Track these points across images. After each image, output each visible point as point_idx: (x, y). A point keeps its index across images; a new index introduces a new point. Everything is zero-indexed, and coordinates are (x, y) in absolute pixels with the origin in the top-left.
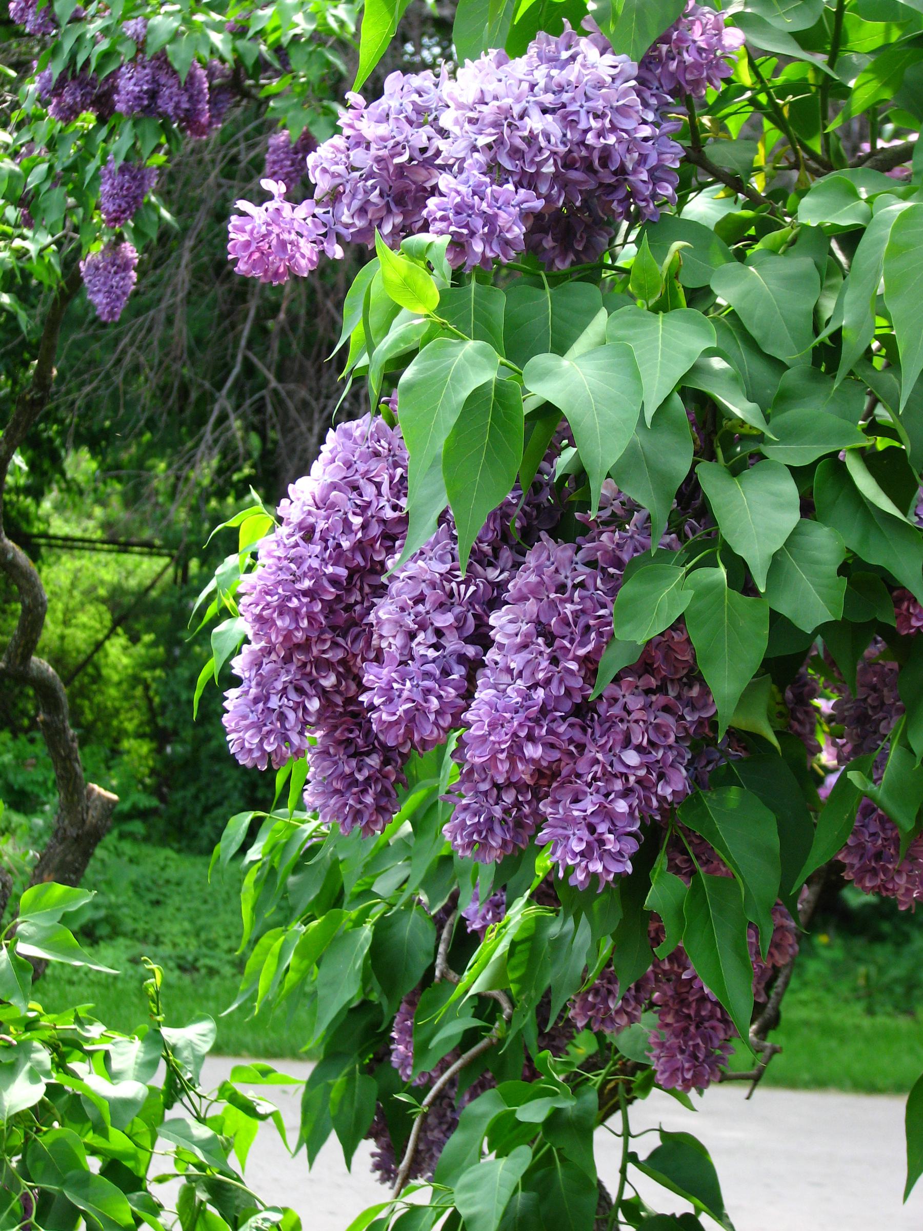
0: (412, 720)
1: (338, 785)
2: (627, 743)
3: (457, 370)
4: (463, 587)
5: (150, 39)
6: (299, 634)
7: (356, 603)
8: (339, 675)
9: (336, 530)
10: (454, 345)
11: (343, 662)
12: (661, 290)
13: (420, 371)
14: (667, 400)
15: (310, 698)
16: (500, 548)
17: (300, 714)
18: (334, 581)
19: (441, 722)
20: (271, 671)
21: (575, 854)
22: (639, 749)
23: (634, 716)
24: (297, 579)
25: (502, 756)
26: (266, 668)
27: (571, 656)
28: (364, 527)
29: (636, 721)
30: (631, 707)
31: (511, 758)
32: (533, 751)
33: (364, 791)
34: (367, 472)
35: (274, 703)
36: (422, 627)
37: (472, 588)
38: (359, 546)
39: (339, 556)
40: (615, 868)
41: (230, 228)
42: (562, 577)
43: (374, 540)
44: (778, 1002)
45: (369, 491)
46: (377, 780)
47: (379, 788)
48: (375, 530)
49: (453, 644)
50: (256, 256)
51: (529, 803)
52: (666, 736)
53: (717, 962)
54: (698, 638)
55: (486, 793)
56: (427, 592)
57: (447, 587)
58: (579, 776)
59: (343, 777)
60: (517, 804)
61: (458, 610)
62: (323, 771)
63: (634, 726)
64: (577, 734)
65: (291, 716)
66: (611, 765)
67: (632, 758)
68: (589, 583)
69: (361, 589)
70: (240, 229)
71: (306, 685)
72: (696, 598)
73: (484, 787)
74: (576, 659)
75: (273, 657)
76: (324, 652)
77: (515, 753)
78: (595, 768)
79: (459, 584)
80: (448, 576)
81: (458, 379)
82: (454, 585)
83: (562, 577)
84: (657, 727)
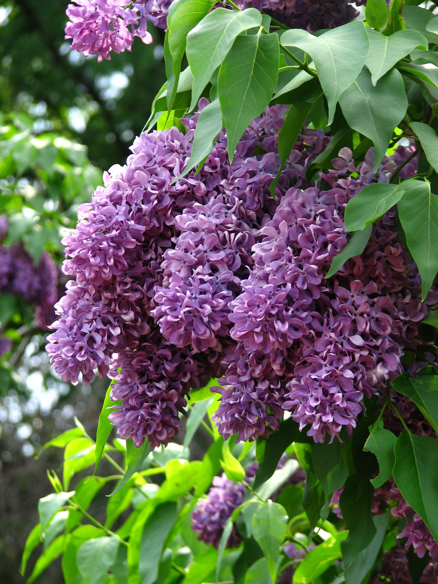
0: (191, 323)
1: (132, 402)
2: (354, 332)
3: (231, 25)
4: (233, 235)
5: (11, 231)
6: (107, 271)
7: (151, 259)
8: (136, 314)
9: (138, 198)
10: (230, 12)
11: (139, 302)
12: (388, 20)
13: (204, 28)
14: (389, 73)
15: (114, 327)
16: (262, 217)
17: (106, 338)
18: (135, 234)
19: (213, 327)
20: (84, 306)
21: (312, 409)
22: (363, 335)
23: (360, 310)
24: (109, 230)
25: (258, 330)
26: (81, 303)
27: (312, 260)
28: (160, 198)
29: (362, 315)
30: (357, 303)
31: (264, 333)
32: (282, 327)
33: (153, 407)
34: (162, 161)
35: (86, 329)
36: (200, 262)
37: (240, 234)
38: (155, 212)
39: (139, 217)
40: (342, 422)
41: (68, 13)
42: (308, 210)
43: (166, 209)
44: (430, 95)
45: (164, 175)
46: (163, 400)
47: (164, 406)
48: (168, 201)
49: (224, 274)
50: (86, 32)
51: (278, 390)
52: (384, 329)
53: (420, 496)
54: (407, 226)
55: (245, 384)
56: (205, 237)
57: (221, 235)
58: (317, 353)
59: (137, 396)
60: (270, 390)
61: (228, 251)
62: (122, 391)
63: (359, 318)
64: (316, 324)
65: (98, 338)
66: (342, 344)
67: (358, 340)
68: (328, 213)
69: (156, 251)
70: (76, 14)
71: (110, 318)
72: (404, 197)
73: (244, 379)
74: (316, 263)
75: (87, 296)
76: (126, 291)
77: (267, 327)
78: (329, 347)
79: (230, 233)
80: (222, 227)
81: (231, 29)
82: (226, 233)
83: (308, 210)
84: (377, 320)
